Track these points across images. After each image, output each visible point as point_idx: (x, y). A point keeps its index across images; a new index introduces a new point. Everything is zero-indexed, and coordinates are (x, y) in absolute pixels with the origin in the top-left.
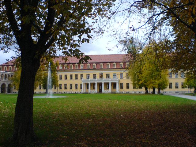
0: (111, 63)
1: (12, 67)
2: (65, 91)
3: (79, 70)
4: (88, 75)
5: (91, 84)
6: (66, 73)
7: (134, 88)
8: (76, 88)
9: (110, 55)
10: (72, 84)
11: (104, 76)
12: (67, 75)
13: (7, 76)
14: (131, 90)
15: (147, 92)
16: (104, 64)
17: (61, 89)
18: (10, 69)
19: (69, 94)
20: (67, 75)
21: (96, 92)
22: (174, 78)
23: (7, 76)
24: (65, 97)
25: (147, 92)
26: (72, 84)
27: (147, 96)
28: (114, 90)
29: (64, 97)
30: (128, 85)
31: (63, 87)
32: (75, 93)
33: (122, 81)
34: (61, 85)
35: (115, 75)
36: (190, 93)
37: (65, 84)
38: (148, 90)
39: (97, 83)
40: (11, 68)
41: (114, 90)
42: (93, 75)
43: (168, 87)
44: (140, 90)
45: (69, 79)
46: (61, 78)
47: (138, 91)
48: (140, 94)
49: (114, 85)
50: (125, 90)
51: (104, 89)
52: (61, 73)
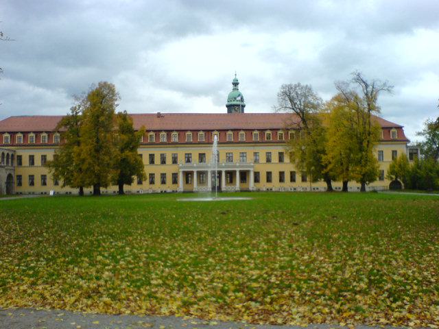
0: (236, 130)
1: (11, 136)
2: (269, 186)
3: (169, 144)
4: (187, 156)
5: (227, 172)
6: (269, 149)
7: (304, 180)
8: (163, 182)
9: (217, 115)
10: (154, 174)
11: (195, 158)
12: (33, 156)
13: (6, 155)
14: (299, 184)
15: (330, 189)
16: (181, 133)
17: (154, 183)
18: (281, 137)
19: (152, 193)
20: (33, 156)
21: (237, 189)
22: (287, 163)
23: (6, 155)
24: (248, 199)
25: (330, 189)
26: (154, 174)
27: (333, 198)
28: (244, 186)
29: (244, 199)
30: (44, 177)
31: (158, 179)
32: (162, 192)
33: (258, 168)
34: (152, 176)
35: (243, 155)
36: (150, 192)
37: (30, 176)
38: (350, 184)
39: (184, 172)
40: (282, 134)
41: (244, 186)
42: (42, 156)
43: (148, 181)
44: (315, 185)
45: (40, 164)
46: (152, 162)
47: (308, 185)
48: (314, 192)
49: (244, 175)
50: (38, 187)
51: (227, 183)
52: (381, 147)
